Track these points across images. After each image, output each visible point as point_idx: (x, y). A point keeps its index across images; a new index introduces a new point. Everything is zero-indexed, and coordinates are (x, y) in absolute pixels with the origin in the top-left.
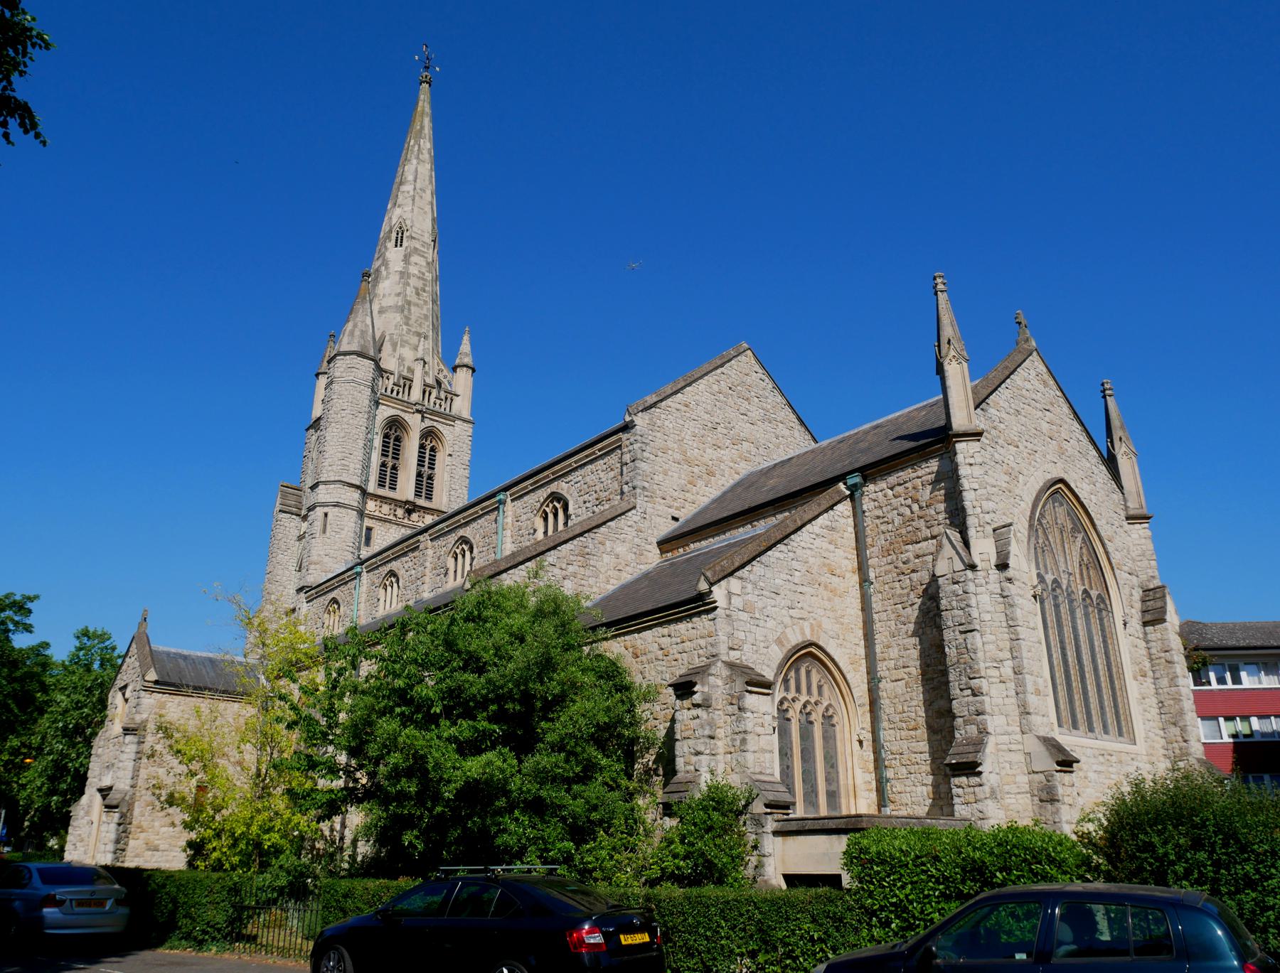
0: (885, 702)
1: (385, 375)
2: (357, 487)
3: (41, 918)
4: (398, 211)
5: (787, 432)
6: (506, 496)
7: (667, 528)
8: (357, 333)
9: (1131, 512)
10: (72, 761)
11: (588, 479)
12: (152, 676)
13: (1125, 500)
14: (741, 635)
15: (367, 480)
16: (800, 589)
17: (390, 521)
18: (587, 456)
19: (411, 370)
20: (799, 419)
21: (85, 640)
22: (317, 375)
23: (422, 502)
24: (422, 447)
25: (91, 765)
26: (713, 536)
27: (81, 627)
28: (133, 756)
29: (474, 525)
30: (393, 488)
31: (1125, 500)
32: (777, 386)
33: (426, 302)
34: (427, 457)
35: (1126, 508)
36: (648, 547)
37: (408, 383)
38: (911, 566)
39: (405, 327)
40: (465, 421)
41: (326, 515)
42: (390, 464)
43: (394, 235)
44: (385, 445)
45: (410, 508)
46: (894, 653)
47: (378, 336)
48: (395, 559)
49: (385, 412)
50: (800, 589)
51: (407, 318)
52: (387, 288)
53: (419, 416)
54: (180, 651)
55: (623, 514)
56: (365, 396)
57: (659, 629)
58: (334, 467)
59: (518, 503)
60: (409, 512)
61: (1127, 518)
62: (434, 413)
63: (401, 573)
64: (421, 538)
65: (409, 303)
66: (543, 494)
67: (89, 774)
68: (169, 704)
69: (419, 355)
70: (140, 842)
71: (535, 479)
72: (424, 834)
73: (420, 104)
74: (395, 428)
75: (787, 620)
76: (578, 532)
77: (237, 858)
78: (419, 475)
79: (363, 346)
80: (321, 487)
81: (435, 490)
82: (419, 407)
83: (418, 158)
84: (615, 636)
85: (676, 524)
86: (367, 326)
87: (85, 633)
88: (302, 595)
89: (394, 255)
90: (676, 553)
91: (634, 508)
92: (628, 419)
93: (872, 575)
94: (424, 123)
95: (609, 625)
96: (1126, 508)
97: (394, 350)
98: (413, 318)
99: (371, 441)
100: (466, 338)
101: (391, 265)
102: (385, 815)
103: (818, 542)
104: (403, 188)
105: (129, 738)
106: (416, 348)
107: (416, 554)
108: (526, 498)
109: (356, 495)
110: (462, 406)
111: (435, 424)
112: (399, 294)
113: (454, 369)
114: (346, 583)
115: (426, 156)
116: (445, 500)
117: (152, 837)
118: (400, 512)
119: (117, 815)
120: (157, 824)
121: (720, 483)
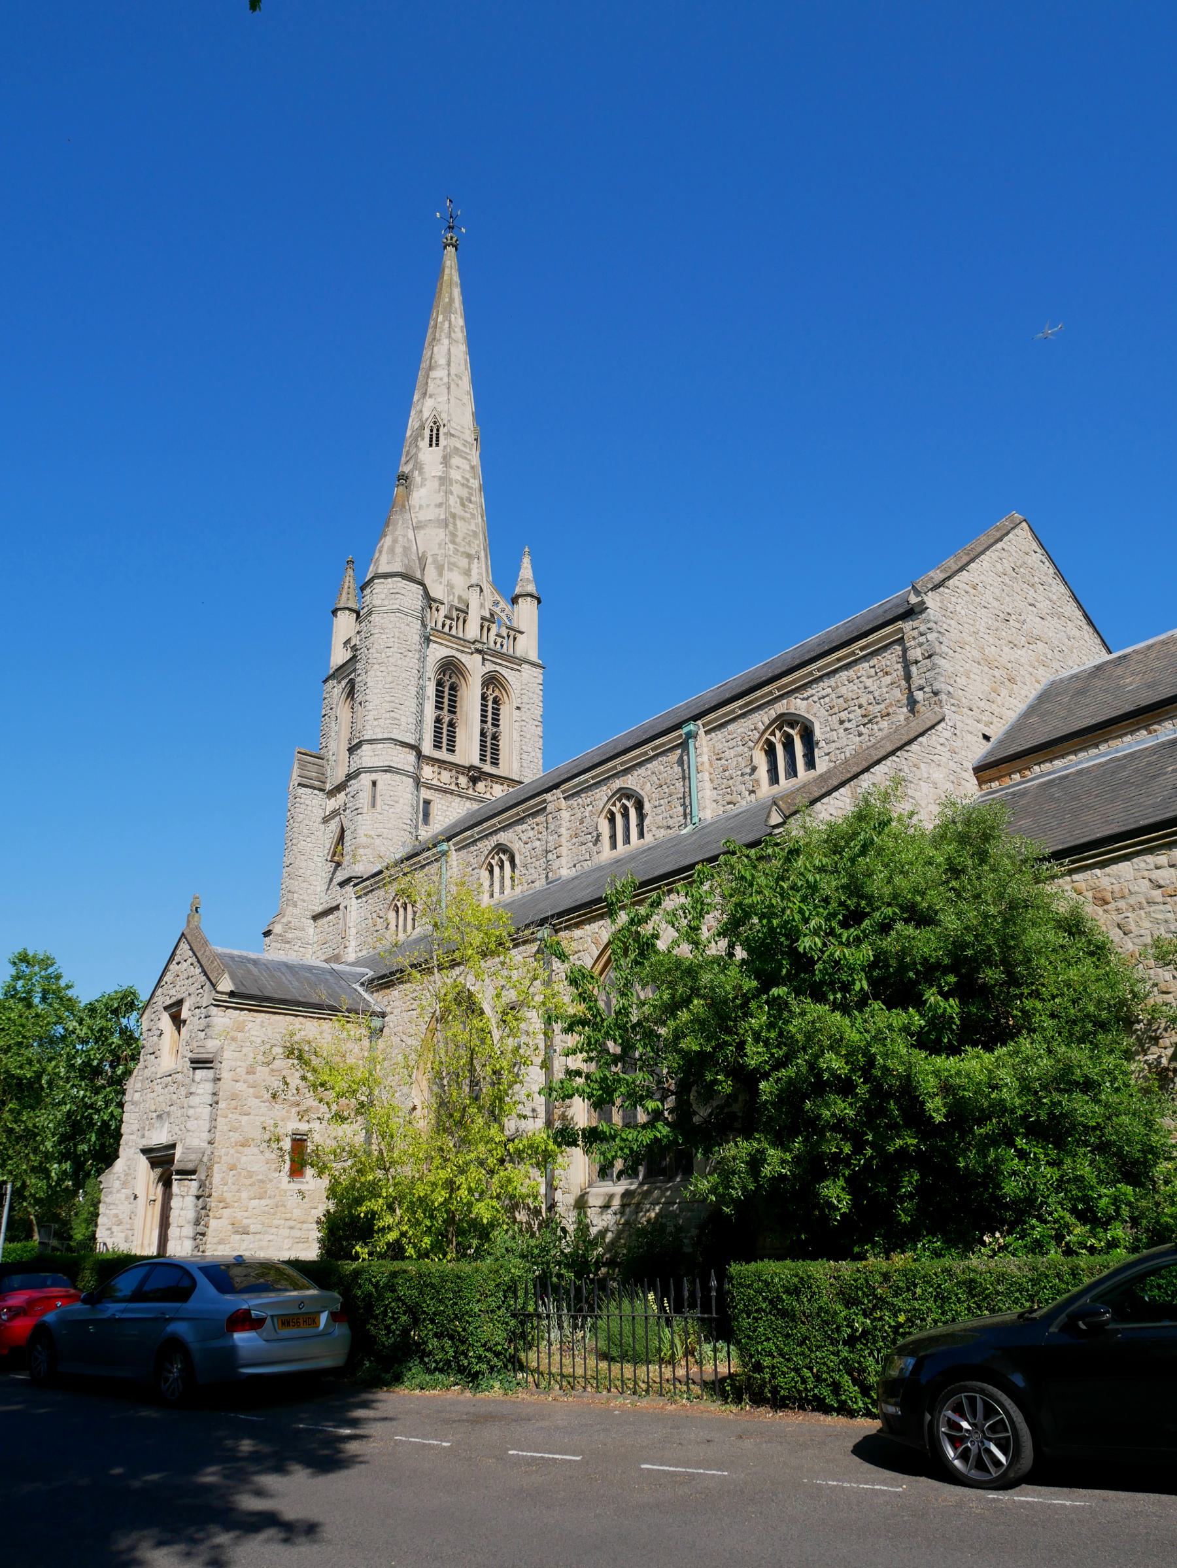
1: (434, 605)
2: (412, 747)
3: (233, 1349)
4: (429, 403)
5: (1077, 633)
6: (698, 727)
7: (979, 751)
10: (98, 1111)
11: (843, 690)
17: (451, 792)
18: (839, 660)
20: (1086, 616)
21: (23, 966)
22: (334, 612)
23: (487, 768)
24: (484, 698)
25: (125, 1117)
26: (1075, 753)
27: (19, 949)
28: (209, 1099)
29: (641, 771)
30: (451, 750)
32: (1059, 573)
33: (473, 515)
34: (491, 712)
36: (965, 775)
37: (462, 615)
39: (451, 546)
40: (533, 664)
41: (374, 783)
42: (446, 720)
43: (427, 432)
44: (439, 695)
45: (476, 776)
48: (503, 829)
49: (438, 652)
51: (454, 535)
52: (424, 497)
53: (479, 657)
54: (244, 953)
55: (933, 727)
56: (414, 631)
57: (1149, 858)
58: (381, 722)
59: (719, 735)
60: (474, 780)
62: (496, 654)
63: (516, 846)
64: (548, 796)
65: (454, 516)
66: (763, 718)
67: (124, 1129)
68: (250, 1025)
69: (474, 581)
70: (224, 1222)
71: (747, 699)
72: (854, 1186)
73: (447, 271)
74: (450, 669)
76: (890, 748)
77: (427, 1240)
78: (483, 734)
80: (365, 747)
81: (501, 753)
82: (479, 646)
83: (449, 337)
84: (1071, 872)
85: (987, 746)
87: (24, 958)
88: (349, 888)
89: (429, 456)
90: (1007, 782)
91: (943, 720)
92: (914, 599)
94: (452, 293)
95: (1058, 855)
97: (441, 574)
98: (460, 534)
99: (422, 688)
100: (526, 562)
101: (426, 468)
102: (788, 1157)
104: (433, 374)
105: (200, 1074)
106: (467, 573)
107: (541, 818)
108: (731, 727)
109: (411, 757)
110: (528, 646)
111: (498, 668)
112: (440, 505)
113: (514, 600)
114: (423, 867)
115: (460, 335)
116: (516, 765)
117: (239, 1215)
118: (463, 780)
119: (195, 1184)
120: (244, 1195)
121: (1024, 693)
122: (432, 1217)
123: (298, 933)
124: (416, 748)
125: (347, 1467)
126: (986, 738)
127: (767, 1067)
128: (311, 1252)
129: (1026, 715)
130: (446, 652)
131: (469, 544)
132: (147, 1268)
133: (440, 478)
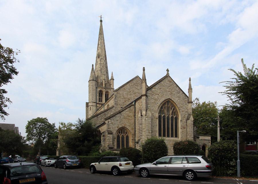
2: (95, 102)
9: (189, 102)
14: (110, 127)
15: (97, 101)
19: (103, 81)
30: (101, 102)
31: (188, 99)
40: (146, 83)
44: (99, 95)
47: (96, 76)
49: (99, 89)
61: (188, 103)
75: (119, 124)
79: (93, 79)
86: (94, 75)
96: (188, 100)
100: (7, 171)
101: (4, 107)
103: (127, 112)
112: (99, 68)
125: (45, 176)
127: (9, 69)
128: (149, 86)
130: (100, 89)
132: (109, 98)
133: (100, 63)
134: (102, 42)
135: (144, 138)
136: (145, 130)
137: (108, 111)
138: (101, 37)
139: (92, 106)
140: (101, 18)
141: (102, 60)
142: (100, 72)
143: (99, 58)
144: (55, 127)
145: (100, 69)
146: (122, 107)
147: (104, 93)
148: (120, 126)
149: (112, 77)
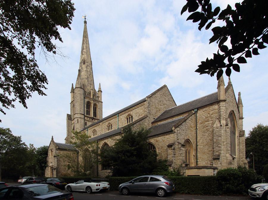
0: (198, 149)
2: (83, 114)
5: (172, 103)
7: (153, 120)
8: (79, 83)
9: (240, 117)
12: (57, 147)
13: (239, 115)
15: (84, 113)
16: (187, 130)
23: (95, 118)
24: (94, 107)
30: (89, 115)
31: (239, 115)
35: (239, 116)
38: (206, 126)
43: (83, 62)
44: (87, 106)
45: (93, 119)
46: (201, 141)
49: (87, 100)
50: (187, 130)
57: (162, 137)
60: (92, 119)
66: (127, 114)
69: (92, 88)
78: (94, 112)
85: (154, 120)
93: (198, 128)
96: (239, 116)
112: (86, 75)
118: (91, 119)
122: (214, 182)
123: (69, 140)
124: (84, 115)
126: (154, 119)
129: (161, 115)
130: (87, 100)
131: (91, 82)
133: (86, 70)
134: (87, 46)
135: (224, 154)
136: (225, 143)
137: (143, 120)
138: (86, 41)
139: (80, 118)
140: (85, 19)
141: (88, 67)
142: (86, 81)
143: (84, 63)
144: (22, 141)
145: (86, 77)
146: (154, 118)
147: (92, 105)
148: (186, 138)
149: (100, 88)
